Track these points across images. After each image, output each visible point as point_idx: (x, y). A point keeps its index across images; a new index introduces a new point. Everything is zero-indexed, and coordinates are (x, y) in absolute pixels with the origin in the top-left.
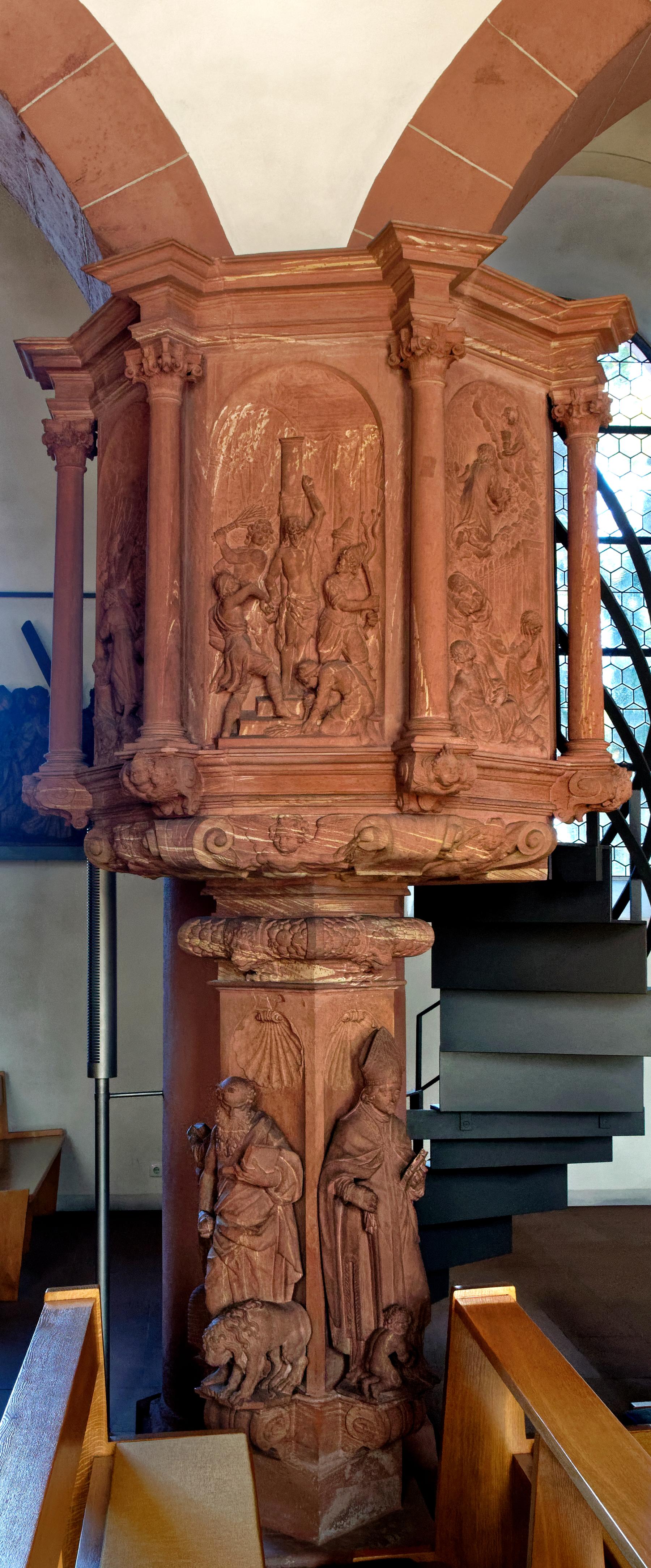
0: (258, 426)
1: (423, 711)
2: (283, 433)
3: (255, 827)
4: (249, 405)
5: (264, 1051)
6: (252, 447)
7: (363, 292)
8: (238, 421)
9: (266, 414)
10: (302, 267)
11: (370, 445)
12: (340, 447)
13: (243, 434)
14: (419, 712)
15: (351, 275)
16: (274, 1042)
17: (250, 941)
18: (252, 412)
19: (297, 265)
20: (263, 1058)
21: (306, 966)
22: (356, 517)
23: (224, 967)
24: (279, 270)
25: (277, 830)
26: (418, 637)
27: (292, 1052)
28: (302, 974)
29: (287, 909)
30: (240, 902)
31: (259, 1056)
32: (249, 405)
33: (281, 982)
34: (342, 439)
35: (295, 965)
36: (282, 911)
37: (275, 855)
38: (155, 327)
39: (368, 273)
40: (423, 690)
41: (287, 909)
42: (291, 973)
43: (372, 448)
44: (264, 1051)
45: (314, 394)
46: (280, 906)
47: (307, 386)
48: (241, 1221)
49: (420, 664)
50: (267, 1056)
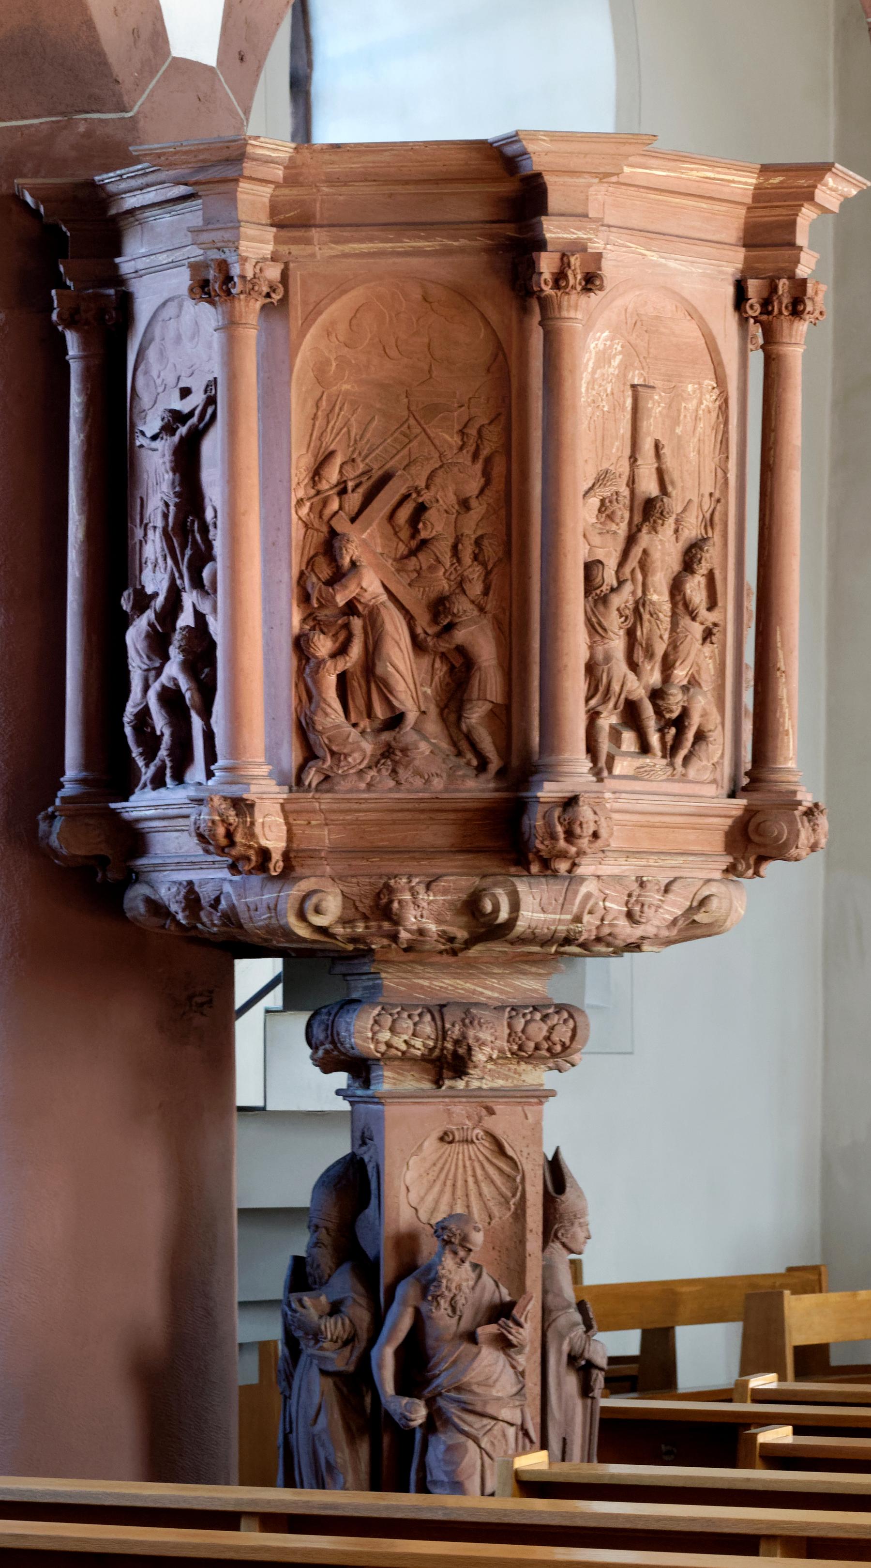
0: (613, 363)
1: (786, 759)
2: (633, 377)
3: (615, 891)
4: (606, 333)
5: (445, 1184)
6: (606, 390)
7: (718, 208)
8: (597, 353)
9: (619, 348)
10: (694, 173)
11: (707, 406)
12: (683, 405)
13: (599, 371)
14: (782, 759)
15: (726, 190)
16: (460, 1170)
17: (492, 1034)
18: (608, 343)
19: (692, 170)
20: (442, 1192)
21: (530, 1067)
22: (696, 500)
23: (392, 1070)
24: (675, 171)
25: (639, 895)
26: (783, 668)
27: (493, 1182)
28: (523, 1077)
29: (502, 992)
30: (426, 983)
31: (436, 1189)
32: (606, 333)
33: (492, 1089)
34: (685, 395)
35: (513, 1067)
36: (496, 995)
37: (624, 926)
38: (579, 229)
39: (739, 191)
40: (787, 735)
41: (502, 992)
42: (506, 1078)
43: (709, 412)
44: (445, 1184)
45: (662, 330)
46: (492, 989)
47: (657, 317)
48: (497, 1392)
49: (785, 702)
50: (448, 1189)
